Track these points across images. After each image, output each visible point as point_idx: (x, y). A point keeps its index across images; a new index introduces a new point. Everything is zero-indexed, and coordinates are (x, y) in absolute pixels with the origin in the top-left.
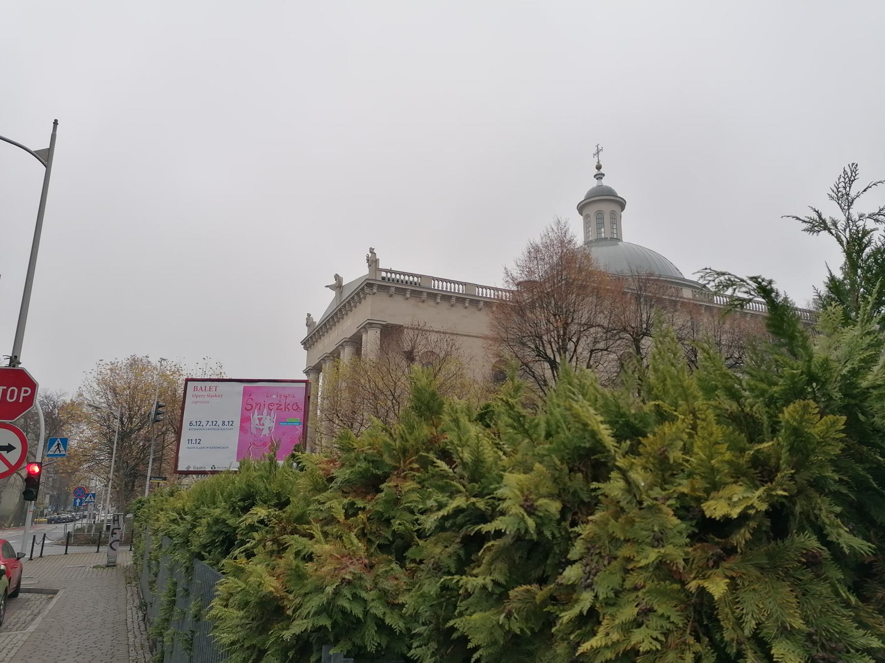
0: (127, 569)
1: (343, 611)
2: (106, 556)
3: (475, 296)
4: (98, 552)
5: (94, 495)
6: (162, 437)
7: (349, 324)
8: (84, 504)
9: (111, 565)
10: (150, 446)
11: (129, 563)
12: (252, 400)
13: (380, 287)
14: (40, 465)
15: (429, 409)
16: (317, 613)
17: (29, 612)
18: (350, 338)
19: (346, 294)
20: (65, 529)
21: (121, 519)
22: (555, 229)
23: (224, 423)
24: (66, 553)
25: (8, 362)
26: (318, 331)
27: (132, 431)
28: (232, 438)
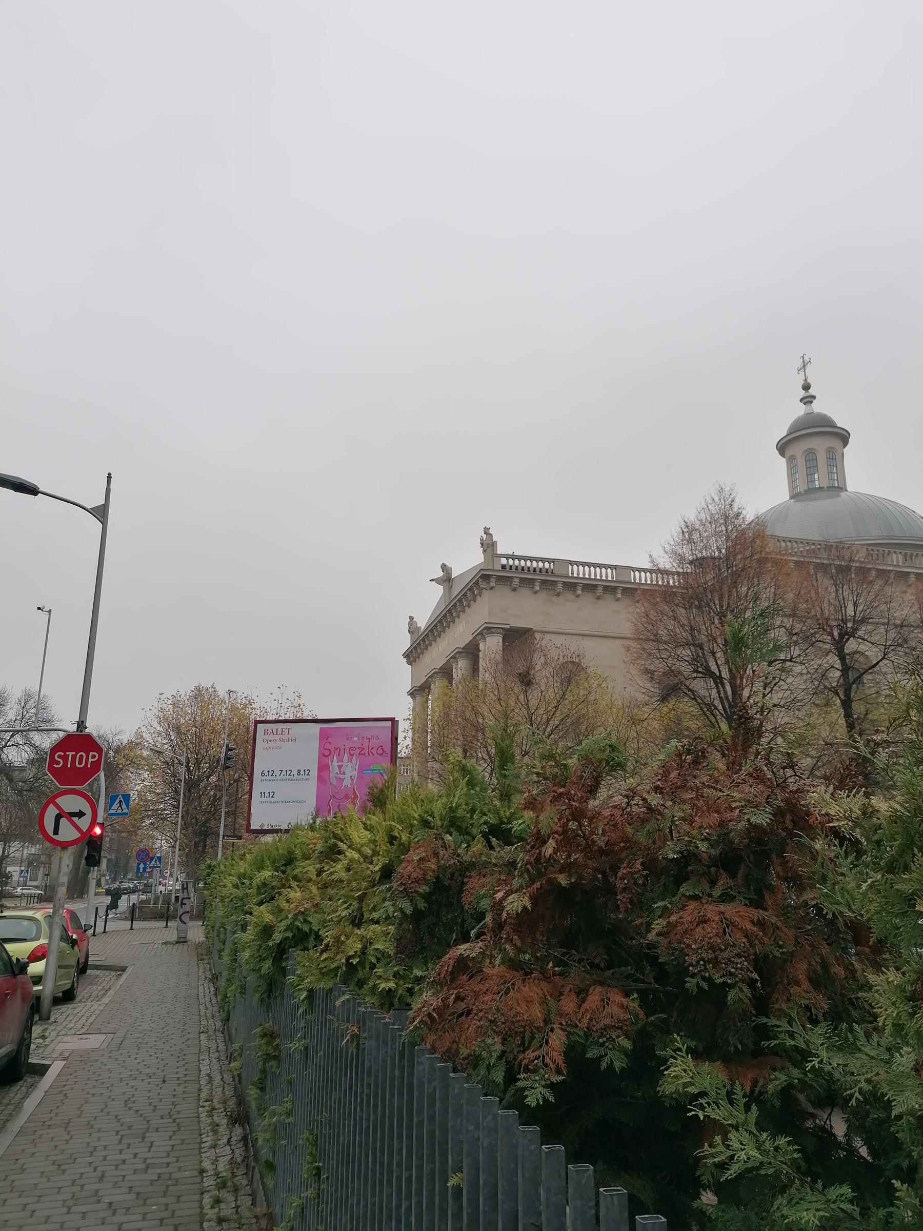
0: (198, 946)
1: (298, 928)
2: (176, 931)
3: (631, 583)
4: (167, 927)
5: (159, 858)
6: (235, 785)
7: (461, 629)
8: (149, 870)
9: (182, 941)
10: (221, 797)
11: (201, 939)
12: (330, 743)
13: (499, 578)
14: (102, 826)
15: (379, 801)
16: (285, 930)
17: (100, 988)
18: (464, 648)
19: (457, 589)
20: (129, 901)
21: (190, 886)
22: (717, 499)
23: (299, 771)
24: (131, 929)
25: (75, 727)
26: (423, 640)
27: (200, 779)
28: (309, 791)
